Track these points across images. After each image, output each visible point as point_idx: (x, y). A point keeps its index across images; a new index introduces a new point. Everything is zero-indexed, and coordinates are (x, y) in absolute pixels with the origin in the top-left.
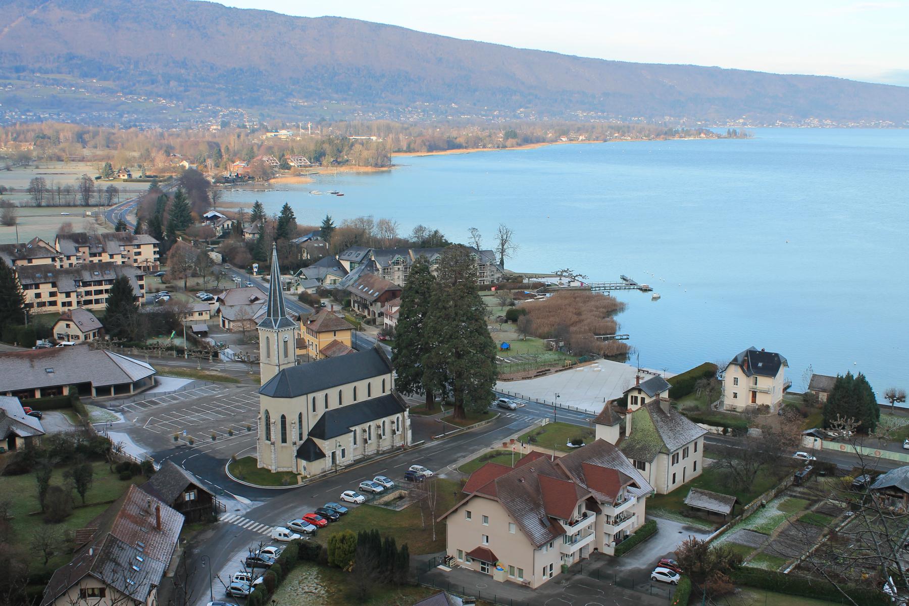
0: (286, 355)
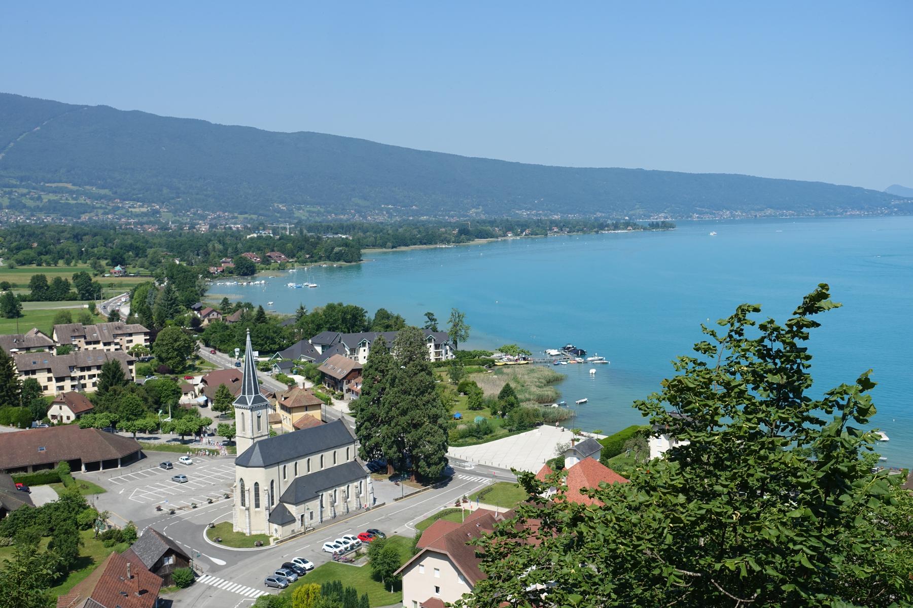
0: (259, 429)
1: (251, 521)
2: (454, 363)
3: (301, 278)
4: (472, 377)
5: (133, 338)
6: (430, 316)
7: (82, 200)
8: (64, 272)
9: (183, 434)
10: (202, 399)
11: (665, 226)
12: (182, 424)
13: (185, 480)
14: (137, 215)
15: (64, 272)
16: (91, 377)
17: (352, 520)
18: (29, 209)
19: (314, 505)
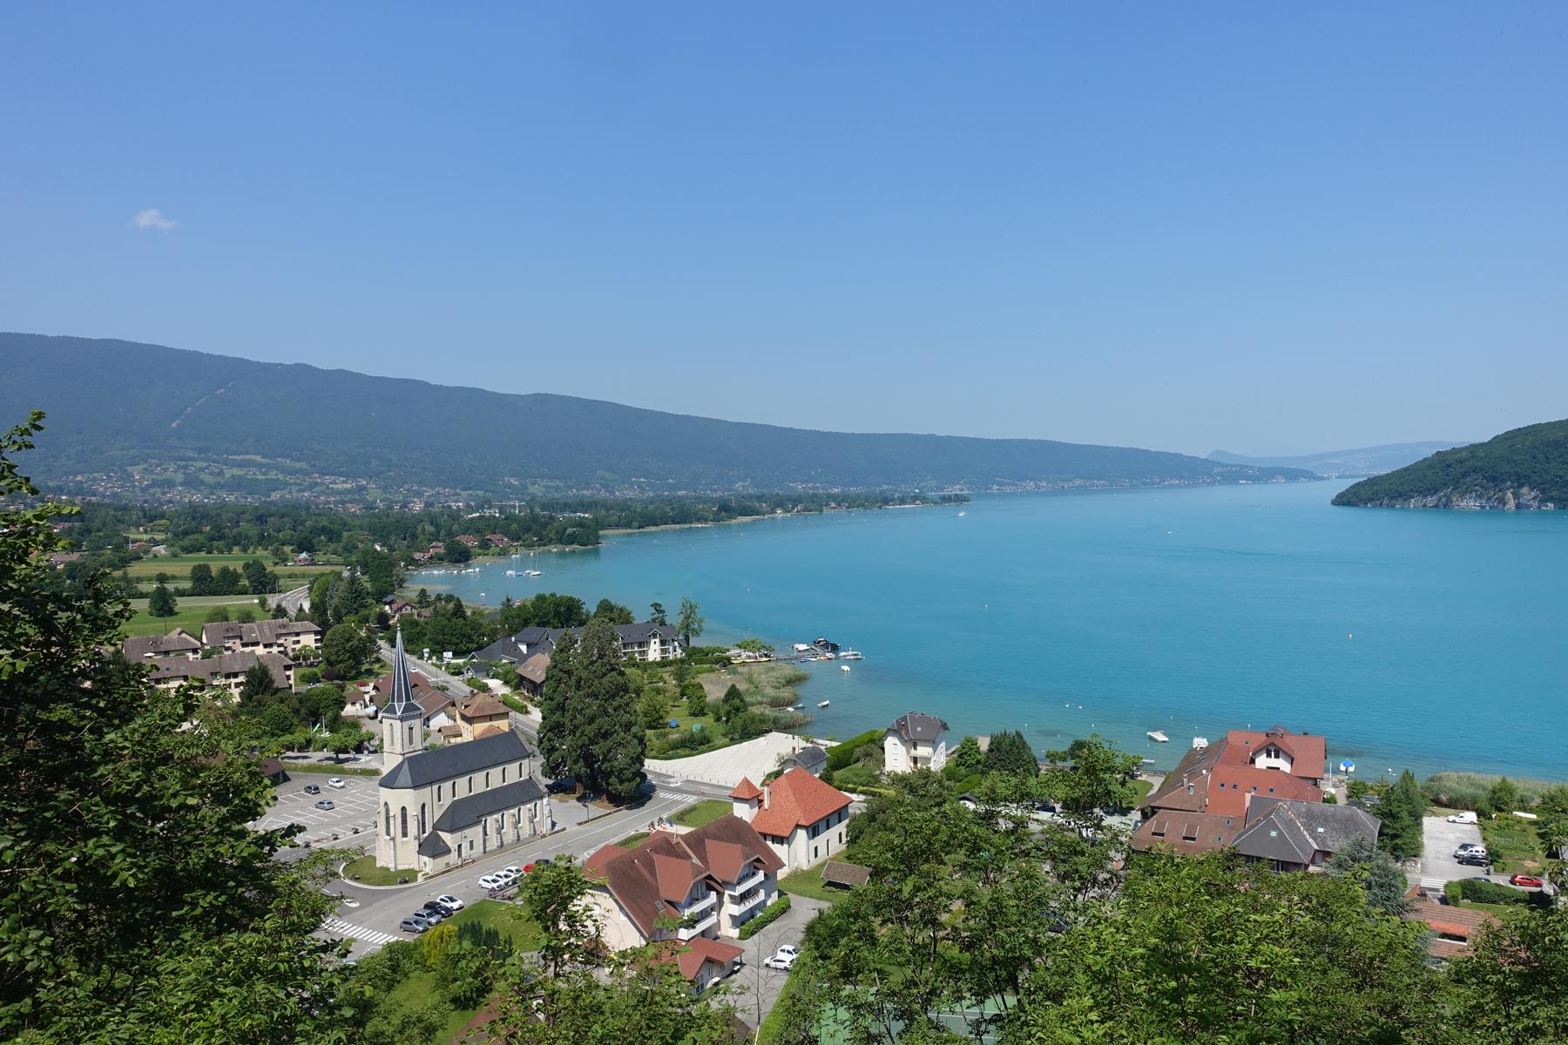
0: (411, 742)
1: (396, 853)
2: (682, 661)
3: (523, 564)
4: (700, 679)
5: (301, 638)
6: (656, 606)
7: (273, 475)
8: (235, 561)
9: (338, 751)
10: (372, 709)
11: (959, 499)
12: (339, 738)
13: (331, 805)
14: (339, 492)
15: (235, 561)
16: (237, 685)
17: (522, 850)
18: (208, 485)
19: (475, 832)
